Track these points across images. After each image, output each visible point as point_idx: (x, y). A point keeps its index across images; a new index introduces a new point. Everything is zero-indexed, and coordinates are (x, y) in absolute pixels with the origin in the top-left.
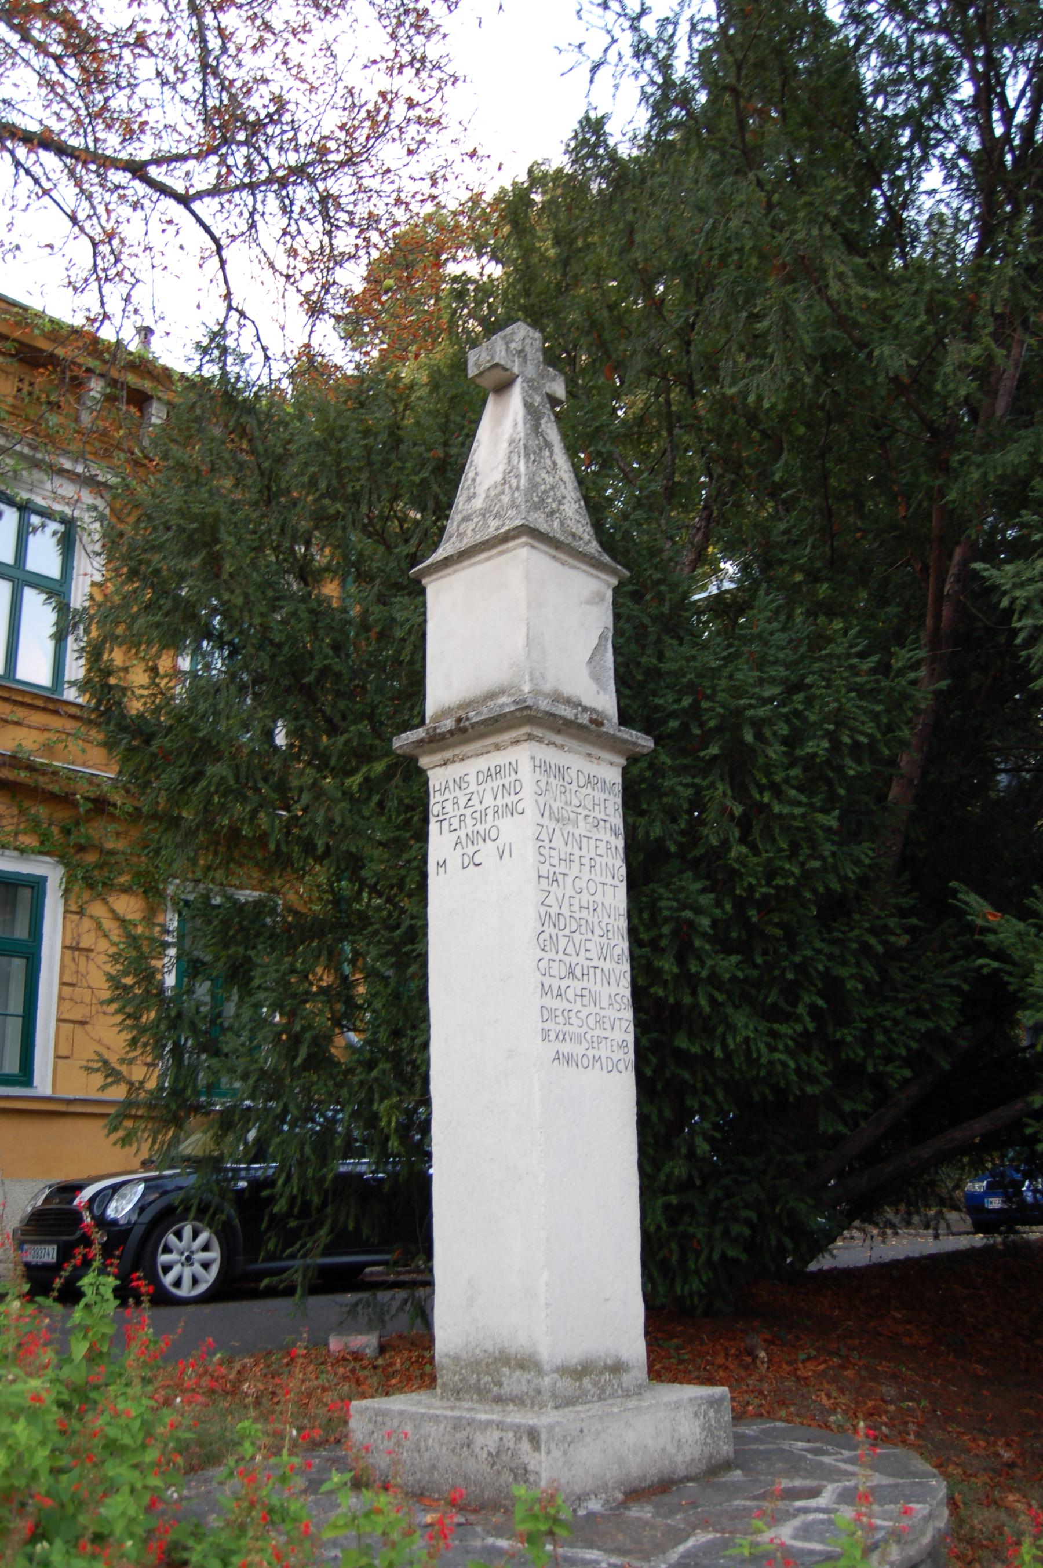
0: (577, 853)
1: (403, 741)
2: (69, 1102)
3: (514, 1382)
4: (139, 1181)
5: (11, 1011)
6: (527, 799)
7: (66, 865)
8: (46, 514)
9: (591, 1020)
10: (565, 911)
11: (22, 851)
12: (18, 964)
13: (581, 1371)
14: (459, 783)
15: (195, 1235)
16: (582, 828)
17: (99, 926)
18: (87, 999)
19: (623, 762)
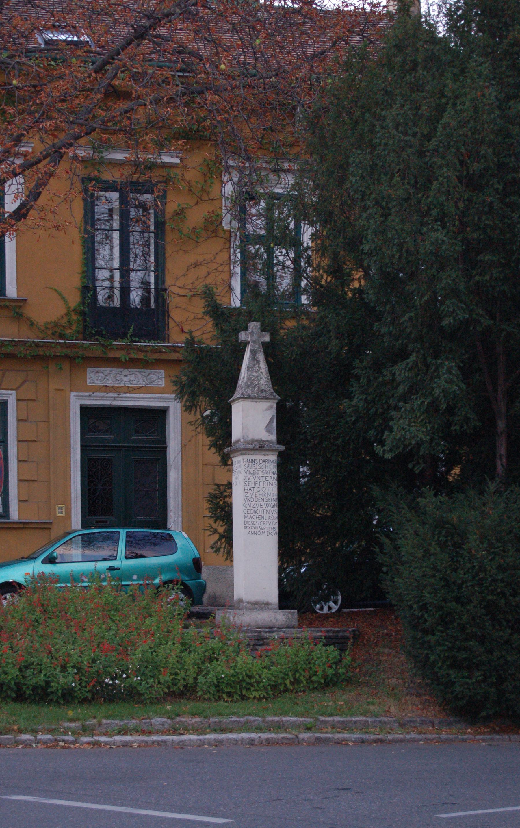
0: (259, 481)
6: (242, 471)
9: (262, 523)
10: (254, 497)
13: (256, 603)
16: (261, 474)
19: (277, 453)
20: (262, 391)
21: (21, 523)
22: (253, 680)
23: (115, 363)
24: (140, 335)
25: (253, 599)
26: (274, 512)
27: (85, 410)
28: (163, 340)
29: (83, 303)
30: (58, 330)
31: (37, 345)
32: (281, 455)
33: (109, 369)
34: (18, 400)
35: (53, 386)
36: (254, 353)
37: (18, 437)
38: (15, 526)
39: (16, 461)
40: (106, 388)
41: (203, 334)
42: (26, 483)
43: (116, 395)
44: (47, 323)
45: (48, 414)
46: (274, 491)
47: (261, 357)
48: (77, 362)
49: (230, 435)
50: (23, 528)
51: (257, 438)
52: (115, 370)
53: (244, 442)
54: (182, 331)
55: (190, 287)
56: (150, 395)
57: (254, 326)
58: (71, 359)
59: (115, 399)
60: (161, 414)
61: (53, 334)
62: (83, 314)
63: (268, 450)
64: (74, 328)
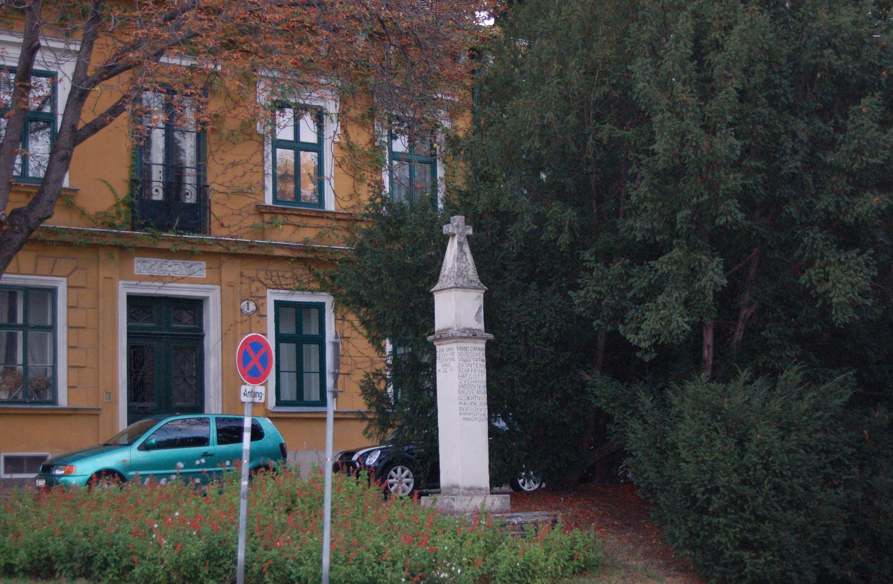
1: (430, 338)
2: (344, 413)
3: (455, 491)
4: (378, 450)
5: (313, 370)
6: (456, 358)
7: (334, 296)
8: (306, 108)
11: (312, 291)
12: (314, 348)
14: (442, 350)
15: (403, 471)
17: (353, 325)
18: (349, 362)
20: (471, 281)
21: (71, 409)
22: (538, 568)
23: (166, 254)
24: (186, 227)
25: (468, 485)
26: (484, 397)
27: (131, 298)
28: (205, 233)
29: (132, 195)
30: (108, 220)
31: (93, 234)
32: (489, 346)
33: (154, 260)
34: (69, 287)
35: (102, 275)
36: (460, 244)
37: (68, 323)
38: (41, 412)
39: (66, 347)
40: (152, 278)
41: (240, 228)
42: (76, 370)
43: (161, 284)
44: (97, 213)
45: (98, 302)
46: (483, 378)
47: (467, 249)
48: (125, 251)
49: (434, 326)
50: (70, 415)
51: (468, 326)
52: (160, 261)
53: (458, 330)
54: (222, 225)
55: (228, 184)
56: (202, 286)
57: (458, 219)
58: (122, 248)
59: (160, 288)
60: (196, 306)
61: (103, 224)
62: (131, 205)
63: (478, 338)
64: (123, 219)
